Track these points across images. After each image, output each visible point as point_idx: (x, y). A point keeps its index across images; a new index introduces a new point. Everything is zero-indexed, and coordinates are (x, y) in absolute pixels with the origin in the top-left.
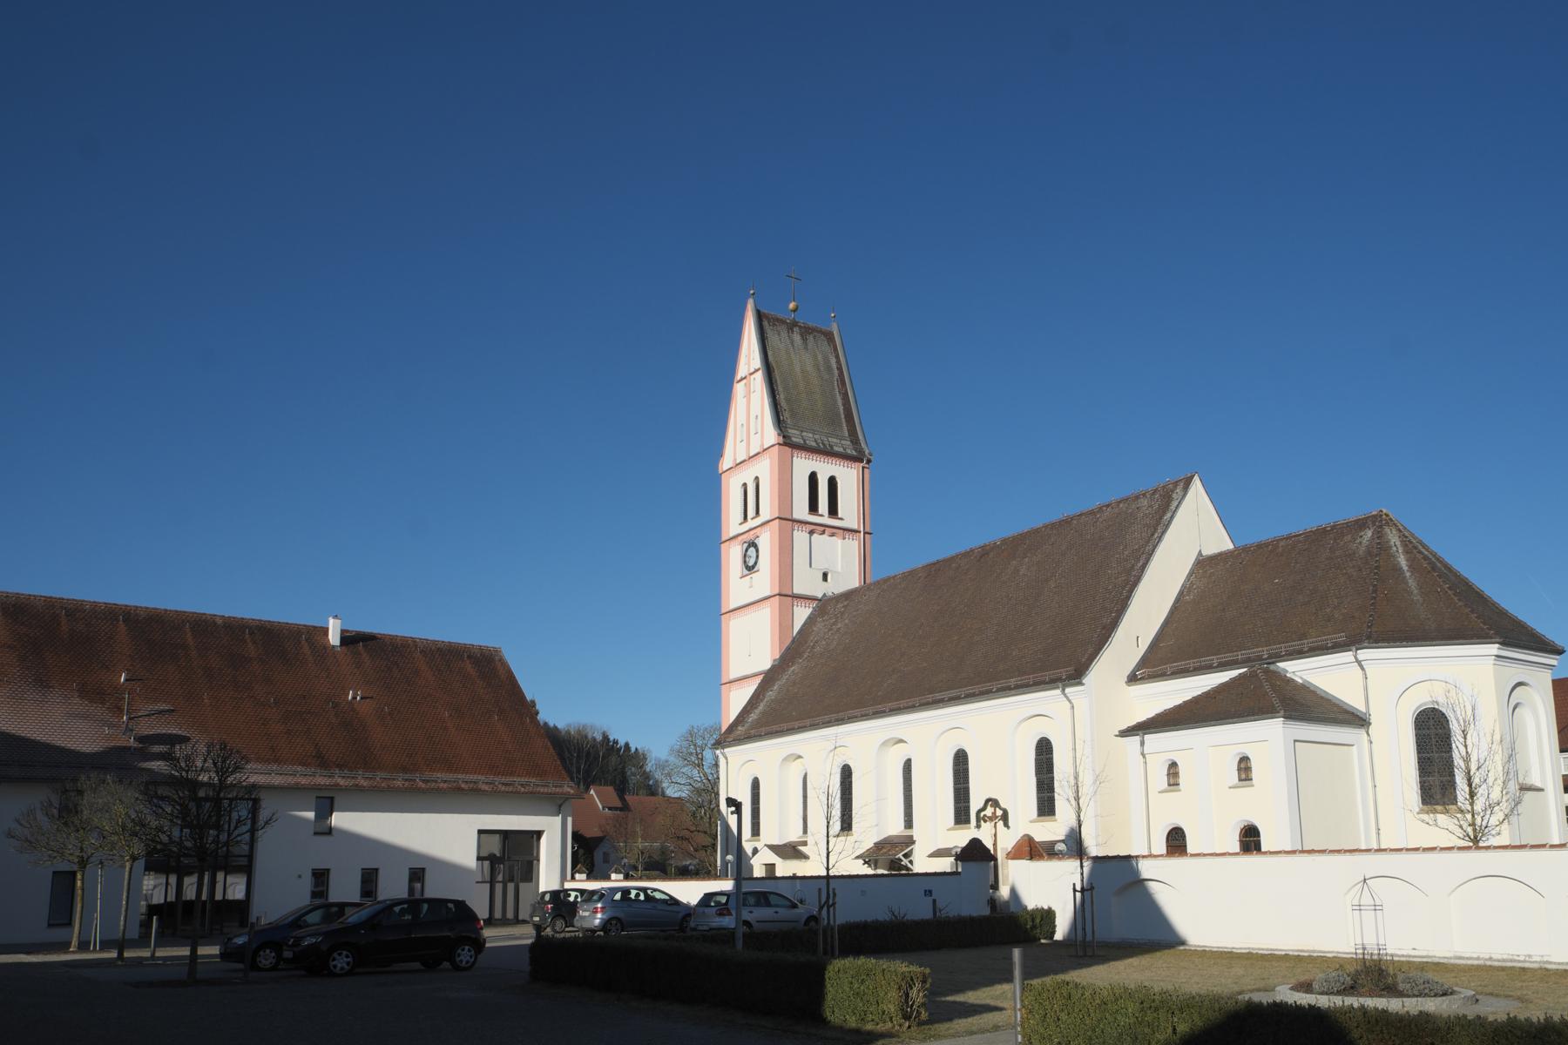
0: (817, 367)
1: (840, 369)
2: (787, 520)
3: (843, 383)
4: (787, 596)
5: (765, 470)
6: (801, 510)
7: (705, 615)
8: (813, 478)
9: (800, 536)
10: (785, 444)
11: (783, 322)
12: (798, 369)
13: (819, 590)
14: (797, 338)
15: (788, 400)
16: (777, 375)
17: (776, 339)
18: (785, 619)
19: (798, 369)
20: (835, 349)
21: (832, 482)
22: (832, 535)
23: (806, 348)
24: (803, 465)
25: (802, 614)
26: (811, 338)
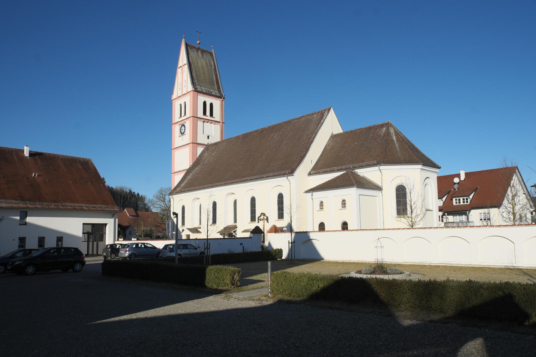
0: (206, 64)
1: (215, 65)
2: (195, 117)
3: (216, 71)
4: (195, 144)
5: (188, 99)
6: (200, 114)
7: (167, 149)
8: (205, 103)
9: (200, 123)
10: (195, 91)
11: (195, 48)
12: (200, 65)
13: (206, 142)
14: (200, 54)
15: (196, 76)
16: (192, 66)
17: (192, 54)
18: (194, 151)
19: (200, 65)
21: (211, 105)
22: (211, 123)
24: (202, 98)
25: (200, 150)
26: (204, 54)
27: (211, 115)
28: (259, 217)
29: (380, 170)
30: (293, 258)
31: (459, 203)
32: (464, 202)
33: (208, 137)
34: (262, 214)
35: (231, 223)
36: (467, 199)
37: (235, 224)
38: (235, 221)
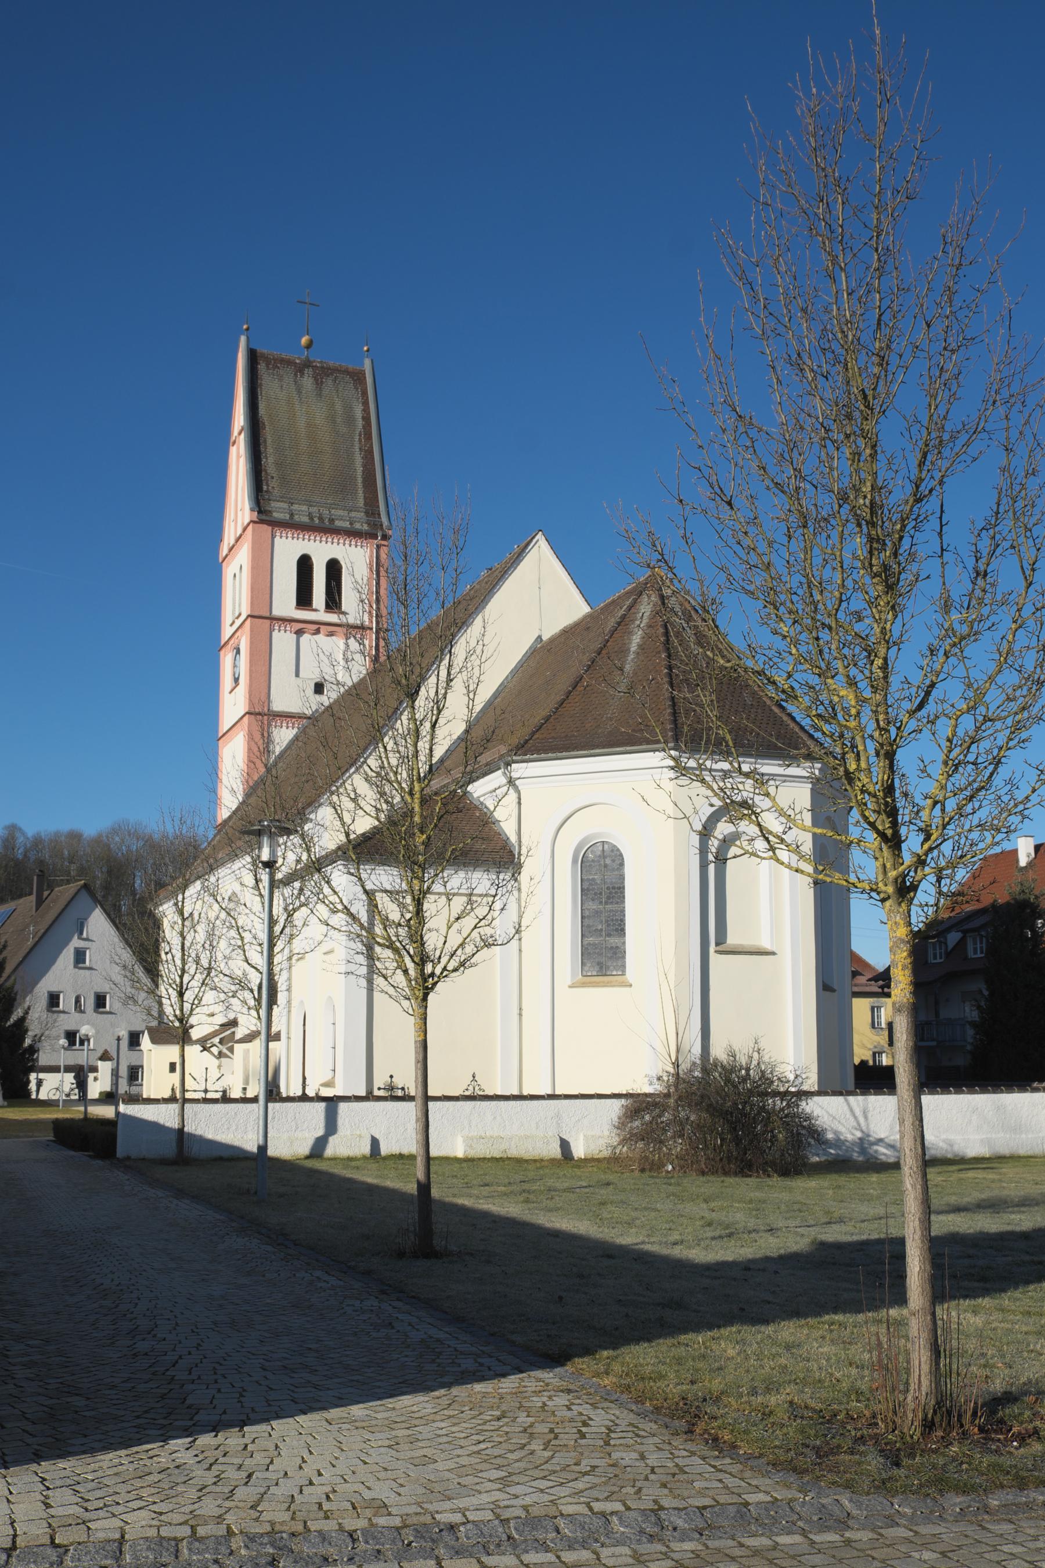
0: (332, 419)
1: (367, 419)
3: (368, 437)
6: (284, 602)
8: (305, 565)
9: (283, 640)
10: (261, 521)
11: (289, 363)
12: (301, 423)
14: (307, 381)
15: (279, 465)
16: (268, 435)
19: (301, 423)
20: (365, 393)
21: (334, 569)
22: (331, 634)
23: (319, 395)
24: (289, 549)
25: (283, 735)
26: (329, 381)
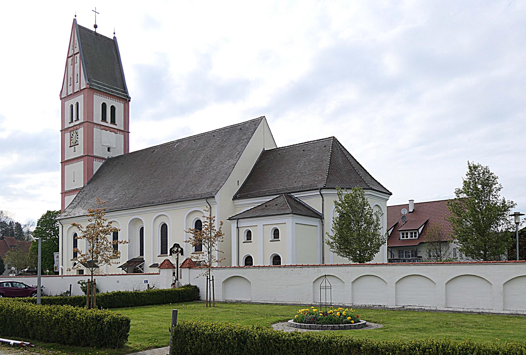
6: (97, 118)
8: (104, 106)
10: (90, 88)
18: (88, 168)
21: (113, 108)
24: (98, 100)
25: (97, 165)
27: (113, 121)
28: (171, 249)
29: (321, 194)
30: (212, 299)
31: (407, 237)
32: (412, 237)
33: (109, 149)
34: (175, 245)
35: (137, 255)
36: (415, 233)
37: (141, 257)
38: (142, 254)
